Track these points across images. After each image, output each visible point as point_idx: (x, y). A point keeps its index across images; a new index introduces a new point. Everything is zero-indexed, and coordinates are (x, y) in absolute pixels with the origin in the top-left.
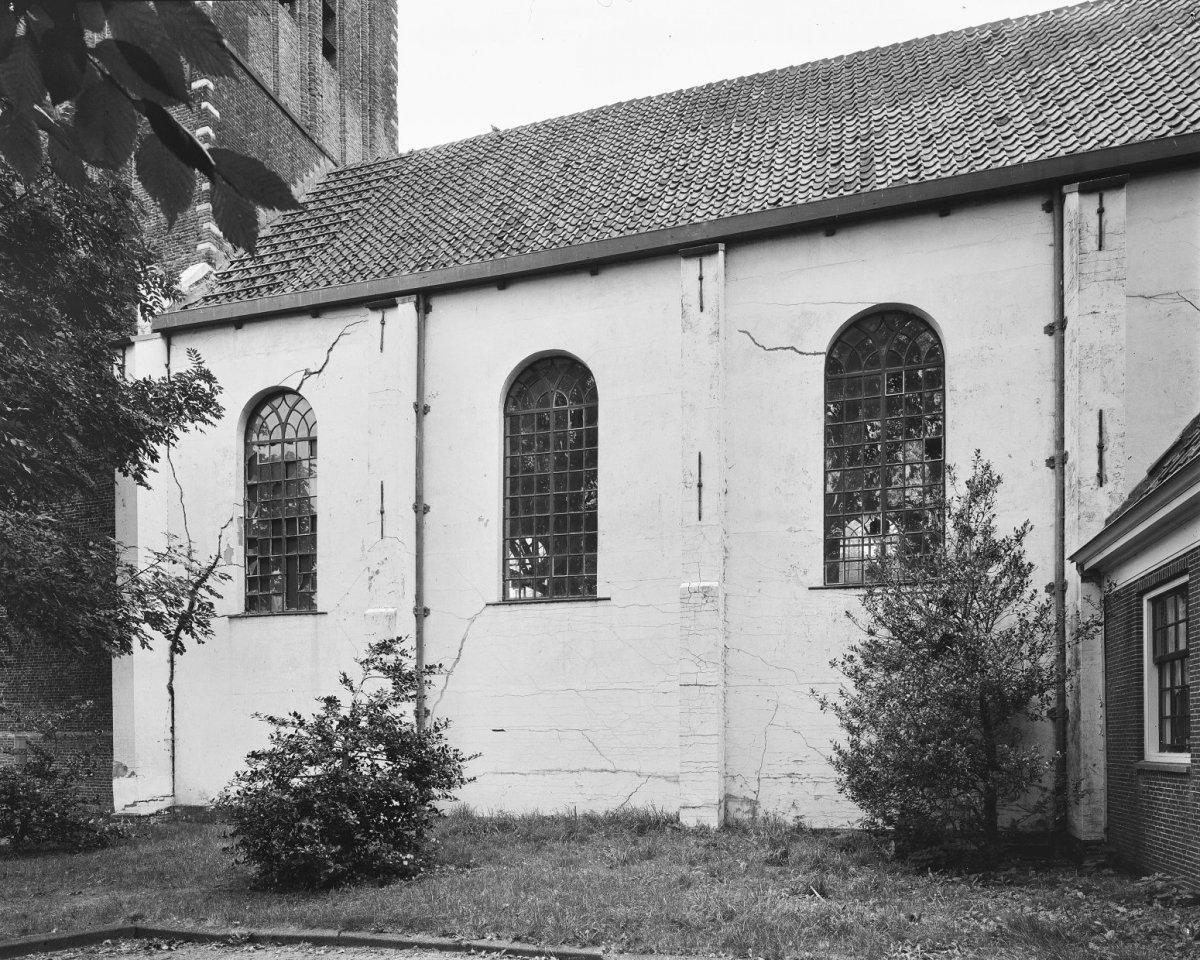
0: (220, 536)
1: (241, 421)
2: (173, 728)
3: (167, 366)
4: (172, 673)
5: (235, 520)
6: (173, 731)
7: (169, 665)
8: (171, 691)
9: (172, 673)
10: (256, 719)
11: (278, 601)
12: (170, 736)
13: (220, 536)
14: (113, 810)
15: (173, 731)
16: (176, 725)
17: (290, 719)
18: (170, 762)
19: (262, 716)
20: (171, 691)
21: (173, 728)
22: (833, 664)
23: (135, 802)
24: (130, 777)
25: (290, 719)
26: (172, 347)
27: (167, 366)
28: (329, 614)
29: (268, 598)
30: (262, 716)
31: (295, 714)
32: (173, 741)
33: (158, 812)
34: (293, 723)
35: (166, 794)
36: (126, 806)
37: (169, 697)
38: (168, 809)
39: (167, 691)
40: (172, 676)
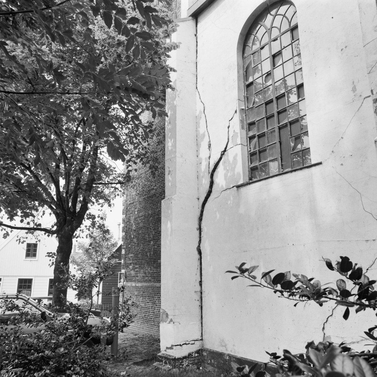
0: (229, 127)
1: (238, 49)
2: (201, 282)
3: (196, 35)
4: (200, 238)
5: (238, 111)
6: (201, 285)
7: (198, 232)
8: (200, 253)
9: (200, 238)
10: (243, 281)
11: (274, 167)
12: (198, 289)
13: (229, 127)
14: (159, 350)
15: (201, 285)
16: (203, 280)
17: (330, 279)
18: (198, 310)
19: (258, 274)
20: (200, 253)
21: (201, 282)
22: (329, 265)
23: (172, 346)
24: (169, 323)
25: (330, 279)
26: (198, 23)
27: (196, 35)
28: (324, 164)
29: (265, 165)
30: (258, 274)
31: (345, 265)
32: (201, 293)
33: (190, 355)
34: (345, 294)
35: (195, 338)
36: (167, 348)
37: (198, 256)
38: (198, 352)
39: (196, 252)
40: (200, 241)
